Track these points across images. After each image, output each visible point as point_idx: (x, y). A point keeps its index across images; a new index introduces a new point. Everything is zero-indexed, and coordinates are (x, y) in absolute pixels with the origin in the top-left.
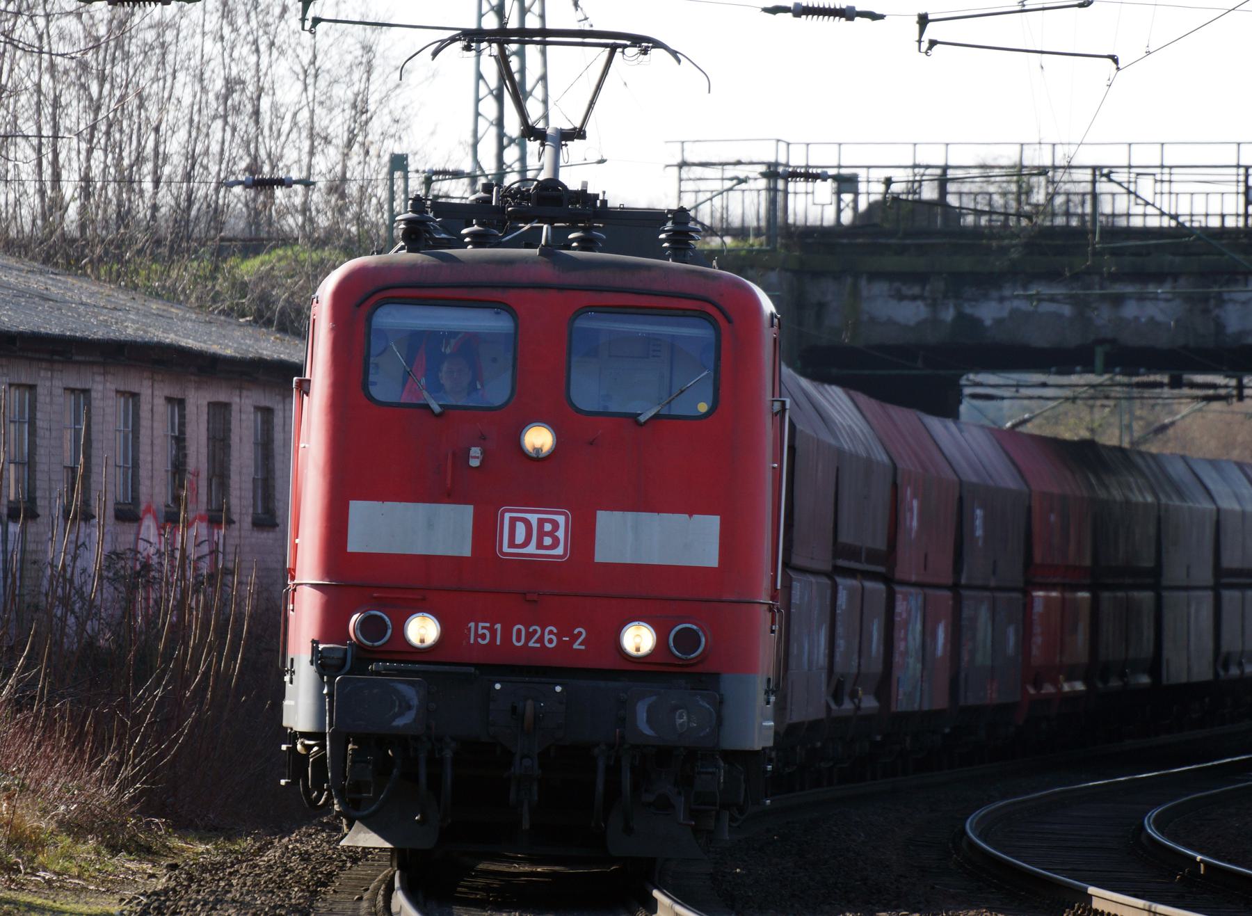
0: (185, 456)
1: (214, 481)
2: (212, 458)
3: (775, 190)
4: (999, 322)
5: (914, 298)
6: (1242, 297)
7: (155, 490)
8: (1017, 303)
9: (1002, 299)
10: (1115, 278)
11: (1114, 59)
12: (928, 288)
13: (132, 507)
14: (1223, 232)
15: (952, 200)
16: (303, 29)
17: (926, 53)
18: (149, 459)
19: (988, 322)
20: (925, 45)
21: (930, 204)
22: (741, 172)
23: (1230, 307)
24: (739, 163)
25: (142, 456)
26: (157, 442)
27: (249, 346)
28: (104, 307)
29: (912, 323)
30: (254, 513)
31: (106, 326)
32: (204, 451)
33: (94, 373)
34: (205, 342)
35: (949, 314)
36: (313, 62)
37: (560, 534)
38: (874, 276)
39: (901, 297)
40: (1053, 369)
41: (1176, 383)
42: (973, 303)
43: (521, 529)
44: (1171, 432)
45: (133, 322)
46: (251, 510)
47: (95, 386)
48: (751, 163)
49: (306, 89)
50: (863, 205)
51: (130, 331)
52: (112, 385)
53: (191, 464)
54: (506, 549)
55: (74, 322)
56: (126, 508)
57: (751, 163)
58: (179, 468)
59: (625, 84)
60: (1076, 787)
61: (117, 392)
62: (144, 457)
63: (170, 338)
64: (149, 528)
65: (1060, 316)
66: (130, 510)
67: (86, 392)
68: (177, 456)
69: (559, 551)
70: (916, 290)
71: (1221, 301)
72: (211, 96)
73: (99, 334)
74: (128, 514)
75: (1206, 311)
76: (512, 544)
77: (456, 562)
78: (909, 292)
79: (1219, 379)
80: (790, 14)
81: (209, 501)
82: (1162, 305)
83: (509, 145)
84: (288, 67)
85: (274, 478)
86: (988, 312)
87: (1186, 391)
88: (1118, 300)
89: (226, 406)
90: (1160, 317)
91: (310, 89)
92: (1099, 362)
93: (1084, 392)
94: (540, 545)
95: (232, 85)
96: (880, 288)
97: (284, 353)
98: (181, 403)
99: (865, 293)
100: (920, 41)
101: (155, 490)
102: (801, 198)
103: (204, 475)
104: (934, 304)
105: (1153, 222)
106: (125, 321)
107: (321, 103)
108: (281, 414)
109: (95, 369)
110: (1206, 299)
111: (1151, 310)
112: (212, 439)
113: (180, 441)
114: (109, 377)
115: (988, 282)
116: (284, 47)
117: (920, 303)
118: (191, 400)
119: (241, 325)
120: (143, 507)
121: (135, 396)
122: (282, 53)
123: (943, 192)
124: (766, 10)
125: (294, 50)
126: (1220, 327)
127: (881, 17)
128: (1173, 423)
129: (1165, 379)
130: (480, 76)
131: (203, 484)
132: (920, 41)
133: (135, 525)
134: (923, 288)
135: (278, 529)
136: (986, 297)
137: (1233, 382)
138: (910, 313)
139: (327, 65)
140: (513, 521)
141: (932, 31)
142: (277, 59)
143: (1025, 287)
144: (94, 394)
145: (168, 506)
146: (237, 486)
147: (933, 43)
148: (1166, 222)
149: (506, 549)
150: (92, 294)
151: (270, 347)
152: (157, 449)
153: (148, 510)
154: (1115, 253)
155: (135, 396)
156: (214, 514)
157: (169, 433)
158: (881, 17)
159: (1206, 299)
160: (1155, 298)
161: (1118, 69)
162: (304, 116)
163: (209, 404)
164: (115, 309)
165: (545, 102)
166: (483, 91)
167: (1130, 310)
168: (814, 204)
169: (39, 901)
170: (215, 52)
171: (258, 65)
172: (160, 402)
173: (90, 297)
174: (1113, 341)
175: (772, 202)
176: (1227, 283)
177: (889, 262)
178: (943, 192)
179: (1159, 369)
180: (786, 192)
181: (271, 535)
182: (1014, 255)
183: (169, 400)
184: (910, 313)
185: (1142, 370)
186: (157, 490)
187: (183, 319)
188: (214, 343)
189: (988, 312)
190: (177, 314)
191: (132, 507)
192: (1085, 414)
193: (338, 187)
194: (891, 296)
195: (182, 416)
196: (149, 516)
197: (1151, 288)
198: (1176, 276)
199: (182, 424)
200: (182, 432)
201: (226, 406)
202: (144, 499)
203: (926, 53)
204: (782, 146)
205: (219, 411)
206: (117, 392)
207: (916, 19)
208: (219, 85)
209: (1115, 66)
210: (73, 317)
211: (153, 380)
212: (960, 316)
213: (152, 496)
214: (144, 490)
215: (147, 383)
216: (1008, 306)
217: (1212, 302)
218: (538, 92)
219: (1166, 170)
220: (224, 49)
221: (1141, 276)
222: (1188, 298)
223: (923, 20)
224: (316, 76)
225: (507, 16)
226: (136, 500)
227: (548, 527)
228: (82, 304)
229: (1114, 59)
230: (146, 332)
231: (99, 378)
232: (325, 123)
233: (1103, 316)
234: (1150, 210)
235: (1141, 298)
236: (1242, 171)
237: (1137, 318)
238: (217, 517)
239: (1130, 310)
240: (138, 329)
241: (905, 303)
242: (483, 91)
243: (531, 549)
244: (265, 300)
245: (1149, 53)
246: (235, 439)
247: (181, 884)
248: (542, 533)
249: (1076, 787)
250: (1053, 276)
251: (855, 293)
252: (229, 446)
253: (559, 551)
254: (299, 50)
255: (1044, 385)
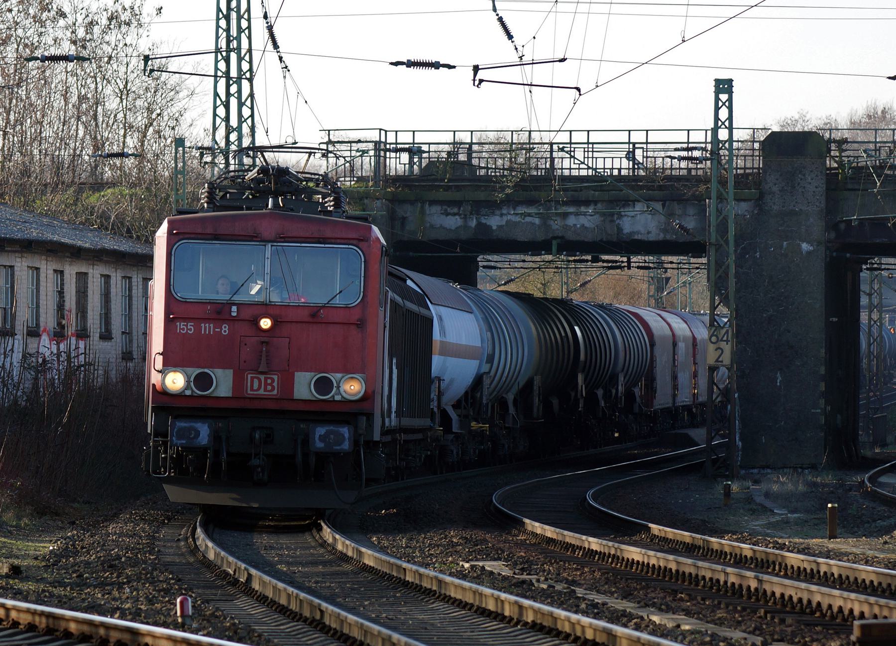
0: (64, 301)
1: (79, 315)
2: (78, 303)
3: (380, 156)
4: (500, 227)
5: (454, 214)
6: (632, 214)
7: (48, 320)
8: (509, 217)
9: (502, 215)
10: (565, 204)
11: (578, 89)
12: (462, 209)
13: (35, 329)
14: (620, 178)
15: (475, 162)
16: (145, 75)
17: (478, 86)
18: (45, 303)
19: (494, 228)
20: (477, 83)
21: (463, 163)
22: (362, 146)
23: (625, 219)
24: (359, 141)
25: (41, 302)
26: (49, 294)
27: (97, 242)
28: (19, 221)
29: (453, 228)
30: (101, 332)
31: (22, 231)
32: (74, 299)
33: (16, 257)
34: (74, 240)
35: (473, 223)
36: (125, 87)
37: (275, 384)
38: (433, 203)
39: (447, 214)
40: (530, 253)
41: (595, 260)
42: (486, 217)
43: (256, 381)
44: (588, 286)
45: (35, 229)
46: (99, 331)
47: (16, 264)
48: (367, 142)
49: (122, 102)
50: (424, 163)
51: (34, 234)
52: (25, 264)
53: (67, 306)
54: (249, 392)
55: (5, 230)
56: (32, 329)
57: (367, 142)
58: (61, 307)
59: (306, 102)
60: (597, 488)
61: (28, 267)
62: (42, 302)
63: (56, 238)
64: (45, 339)
65: (534, 224)
66: (35, 330)
67: (12, 267)
68: (60, 301)
69: (275, 392)
70: (455, 210)
71: (620, 216)
72: (70, 106)
73: (19, 236)
74: (34, 333)
75: (612, 221)
76: (252, 389)
77: (297, 371)
78: (452, 211)
79: (618, 258)
80: (405, 66)
81: (77, 326)
82: (589, 218)
83: (233, 131)
84: (112, 90)
85: (111, 313)
86: (494, 222)
87: (600, 264)
88: (565, 215)
89: (86, 274)
90: (587, 225)
91: (125, 101)
92: (554, 248)
93: (543, 265)
94: (265, 390)
95: (82, 98)
96: (436, 209)
97: (115, 245)
98: (62, 272)
99: (428, 212)
100: (474, 80)
101: (72, 323)
102: (393, 160)
103: (74, 311)
104: (465, 218)
105: (584, 173)
106: (31, 228)
107: (130, 110)
108: (115, 279)
109: (17, 255)
110: (612, 215)
111: (583, 220)
112: (78, 292)
113: (61, 293)
114: (24, 259)
115: (493, 206)
116: (110, 79)
117: (457, 217)
118: (67, 271)
119: (91, 230)
120: (42, 329)
121: (37, 269)
122: (109, 82)
123: (470, 157)
124: (392, 64)
125: (116, 81)
126: (620, 229)
127: (454, 67)
128: (591, 280)
129: (589, 258)
130: (216, 95)
131: (73, 316)
132: (474, 80)
133: (38, 338)
134: (459, 209)
135: (113, 340)
136: (493, 214)
137: (625, 259)
138: (452, 222)
139: (134, 89)
140: (252, 378)
141: (481, 75)
142: (106, 85)
143: (514, 209)
144: (16, 268)
145: (55, 328)
146: (92, 317)
147: (481, 81)
148: (590, 172)
149: (249, 392)
150: (12, 214)
151: (140, 249)
152: (49, 298)
153: (45, 330)
154: (565, 190)
155: (37, 269)
156: (79, 332)
157: (55, 289)
158: (454, 67)
159: (612, 215)
160: (585, 214)
161: (580, 95)
162: (120, 116)
163: (76, 273)
164: (25, 222)
165: (252, 108)
166: (218, 102)
167: (571, 221)
168: (400, 164)
169: (9, 541)
170: (73, 82)
171: (96, 88)
172: (51, 272)
173: (11, 216)
174: (562, 238)
175: (377, 163)
176: (624, 206)
177: (442, 195)
178: (470, 157)
179: (587, 253)
180: (385, 157)
181: (109, 344)
182: (508, 191)
183: (55, 271)
184: (452, 222)
185: (578, 253)
186: (49, 320)
187: (61, 227)
188: (79, 240)
189: (494, 222)
190: (57, 224)
191: (35, 329)
192: (541, 276)
193: (140, 156)
194: (441, 213)
195: (62, 280)
196: (45, 334)
197: (583, 209)
198: (596, 202)
199: (62, 284)
200: (62, 289)
201: (86, 274)
202: (42, 324)
203: (478, 86)
204: (383, 133)
205: (82, 277)
206: (28, 267)
207: (472, 68)
208: (74, 99)
209: (578, 93)
210: (4, 226)
211: (47, 261)
212: (479, 224)
213: (46, 323)
214: (42, 319)
215: (44, 262)
216: (505, 218)
217: (616, 216)
218: (218, 121)
219: (590, 146)
220: (78, 80)
221: (576, 202)
222: (603, 215)
223: (476, 69)
224: (128, 94)
225: (255, 72)
226: (38, 325)
227: (269, 381)
228: (8, 219)
229: (578, 89)
230: (43, 234)
231: (19, 260)
232: (132, 120)
233: (556, 225)
234: (582, 166)
235: (577, 214)
236: (631, 146)
237: (575, 225)
238: (83, 334)
239: (571, 221)
240: (38, 233)
241: (449, 217)
242: (218, 102)
243: (262, 392)
244: (104, 216)
245: (597, 86)
246: (90, 293)
247: (475, 554)
248: (266, 384)
249: (597, 488)
250: (531, 202)
251: (423, 212)
252: (87, 296)
253: (275, 392)
254: (118, 81)
255: (524, 261)
